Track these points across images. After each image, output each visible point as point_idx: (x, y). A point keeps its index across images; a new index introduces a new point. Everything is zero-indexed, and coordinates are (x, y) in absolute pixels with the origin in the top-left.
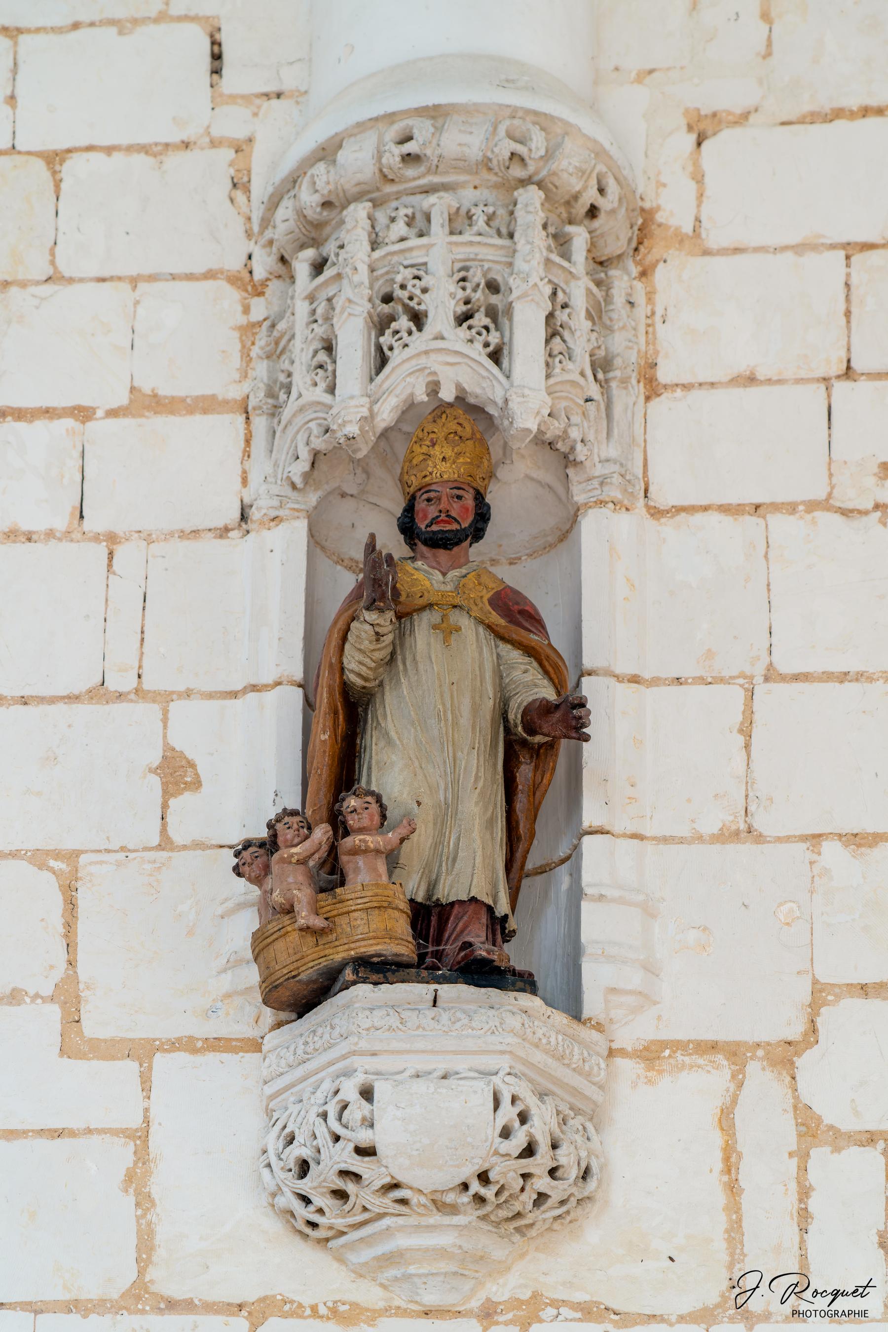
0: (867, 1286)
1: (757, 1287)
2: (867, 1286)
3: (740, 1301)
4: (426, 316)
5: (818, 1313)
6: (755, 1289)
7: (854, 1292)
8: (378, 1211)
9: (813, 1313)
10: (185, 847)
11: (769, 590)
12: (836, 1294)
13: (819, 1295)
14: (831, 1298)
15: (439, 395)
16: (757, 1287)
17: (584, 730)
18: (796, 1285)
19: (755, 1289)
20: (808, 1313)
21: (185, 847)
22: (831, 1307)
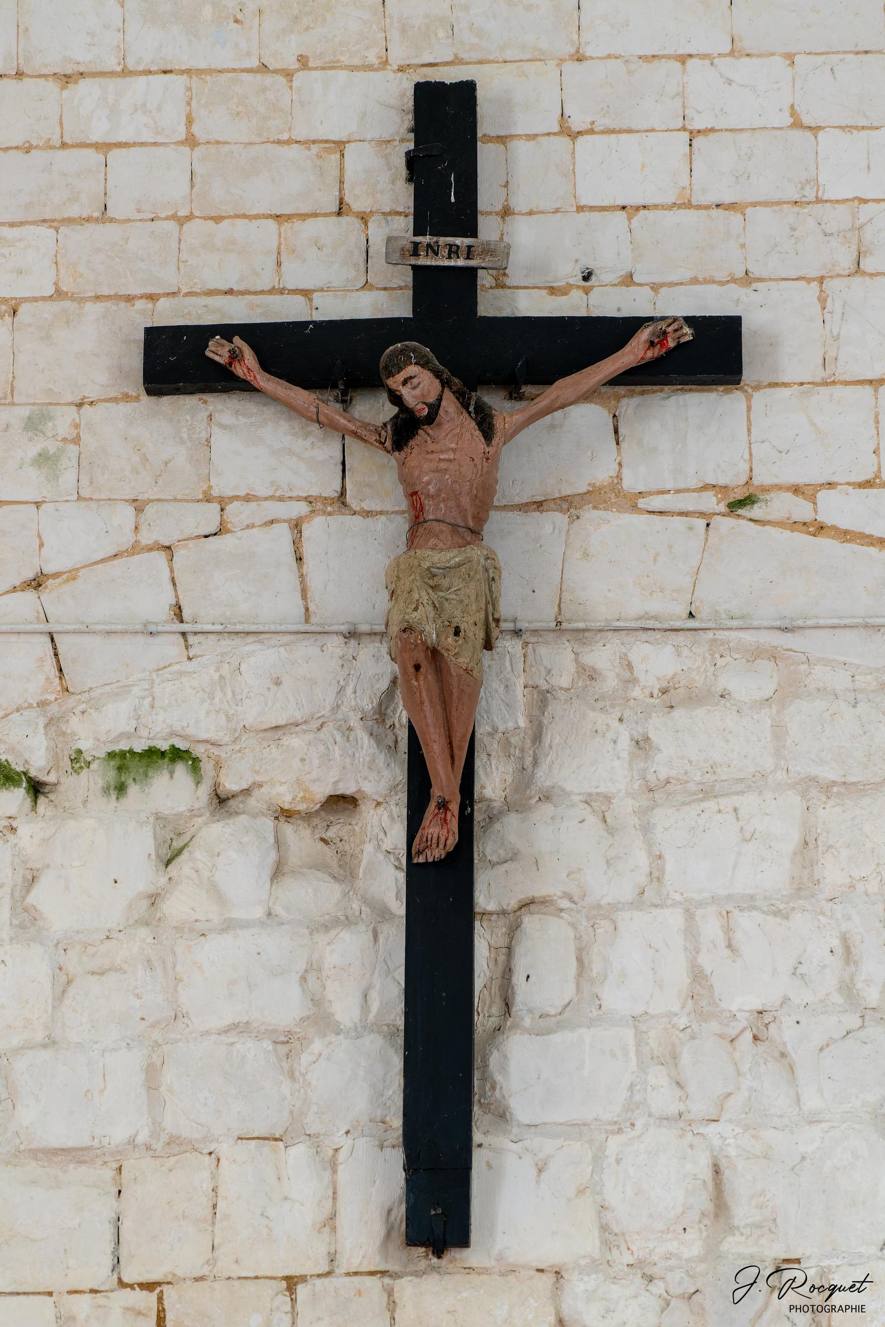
0: (864, 1281)
1: (755, 1282)
2: (864, 1281)
3: (739, 1294)
4: (511, 397)
5: (815, 1308)
6: (752, 1284)
7: (851, 1287)
8: (433, 594)
9: (810, 1308)
10: (646, 285)
11: (174, 584)
12: (833, 1289)
13: (816, 1290)
14: (828, 1293)
15: (491, 304)
16: (755, 1282)
17: (51, 452)
18: (794, 1280)
19: (752, 1284)
20: (806, 1309)
21: (646, 285)
22: (828, 1303)
